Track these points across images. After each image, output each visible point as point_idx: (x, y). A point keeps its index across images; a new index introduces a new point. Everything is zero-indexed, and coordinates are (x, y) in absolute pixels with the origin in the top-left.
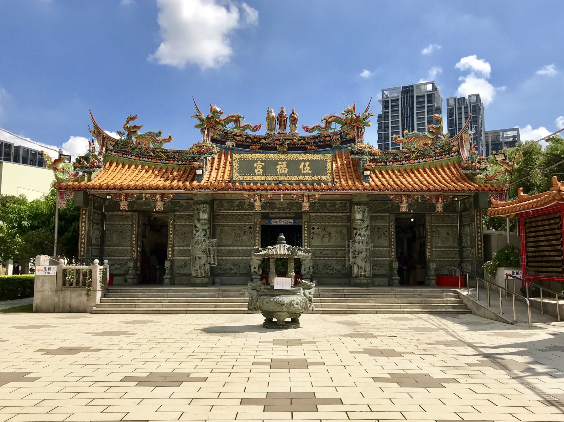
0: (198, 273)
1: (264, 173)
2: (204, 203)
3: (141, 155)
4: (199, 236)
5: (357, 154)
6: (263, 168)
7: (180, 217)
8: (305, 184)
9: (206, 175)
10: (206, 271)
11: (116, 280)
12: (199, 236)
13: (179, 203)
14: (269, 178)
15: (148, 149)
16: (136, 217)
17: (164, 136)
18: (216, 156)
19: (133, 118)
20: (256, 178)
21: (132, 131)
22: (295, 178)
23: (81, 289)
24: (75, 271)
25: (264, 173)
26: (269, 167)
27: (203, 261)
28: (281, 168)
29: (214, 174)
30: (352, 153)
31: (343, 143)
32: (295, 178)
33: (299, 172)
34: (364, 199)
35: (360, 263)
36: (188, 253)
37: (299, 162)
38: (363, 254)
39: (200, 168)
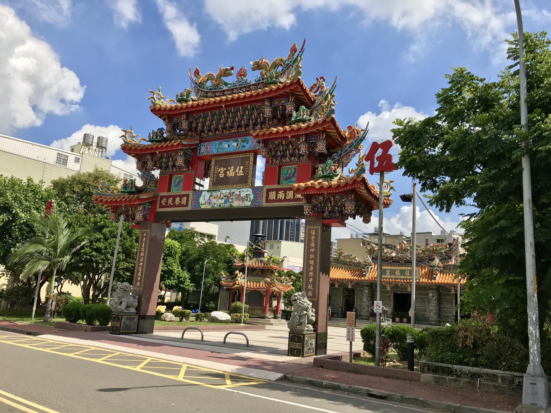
0: (364, 315)
1: (390, 275)
2: (367, 286)
3: (344, 264)
4: (365, 299)
5: (432, 267)
6: (390, 272)
7: (360, 290)
8: (407, 280)
9: (367, 275)
10: (368, 314)
11: (334, 315)
12: (365, 299)
13: (358, 284)
14: (392, 277)
15: (347, 262)
16: (342, 290)
17: (353, 256)
18: (373, 266)
19: (340, 250)
20: (387, 276)
21: (340, 254)
22: (403, 277)
23: (421, 394)
24: (418, 297)
25: (390, 275)
26: (393, 272)
27: (366, 310)
28: (397, 273)
29: (372, 274)
30: (430, 266)
31: (430, 260)
32: (403, 277)
33: (405, 275)
34: (434, 287)
35: (432, 315)
36: (361, 306)
37: (405, 270)
38: (434, 311)
39: (365, 272)
